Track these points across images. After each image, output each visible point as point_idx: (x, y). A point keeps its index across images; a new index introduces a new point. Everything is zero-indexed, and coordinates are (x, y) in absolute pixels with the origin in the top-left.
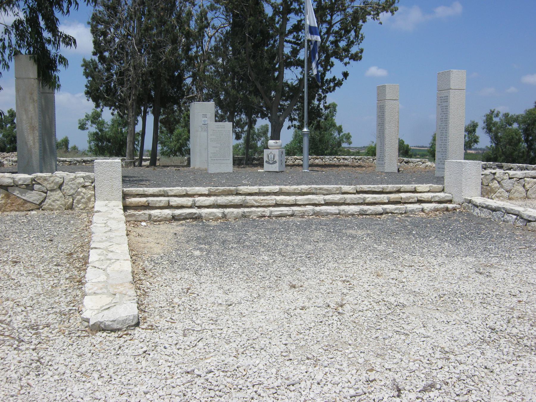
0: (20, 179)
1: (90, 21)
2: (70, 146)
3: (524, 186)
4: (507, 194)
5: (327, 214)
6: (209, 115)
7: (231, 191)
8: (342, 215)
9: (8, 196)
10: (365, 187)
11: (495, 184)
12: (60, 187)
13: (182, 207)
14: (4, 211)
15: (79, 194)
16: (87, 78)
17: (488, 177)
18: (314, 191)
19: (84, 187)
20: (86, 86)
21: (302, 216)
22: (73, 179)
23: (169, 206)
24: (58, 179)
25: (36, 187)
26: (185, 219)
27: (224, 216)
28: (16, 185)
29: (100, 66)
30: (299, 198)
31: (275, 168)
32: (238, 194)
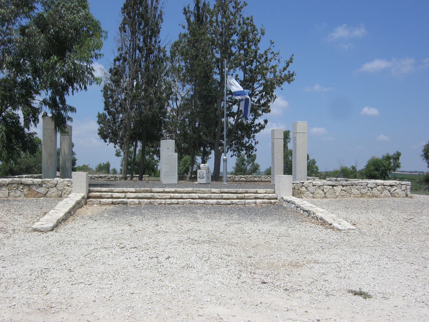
0: (36, 181)
1: (103, 89)
2: (111, 168)
3: (323, 190)
4: (312, 195)
5: (198, 203)
6: (171, 148)
7: (148, 190)
8: (206, 204)
9: (30, 190)
10: (226, 190)
11: (304, 189)
12: (56, 185)
13: (119, 198)
14: (27, 197)
15: (65, 189)
16: (99, 124)
17: (298, 185)
18: (195, 191)
19: (68, 186)
20: (99, 130)
21: (183, 204)
22: (62, 182)
23: (112, 198)
24: (54, 182)
25: (44, 185)
26: (119, 204)
27: (140, 203)
28: (34, 184)
29: (108, 117)
30: (183, 195)
31: (204, 181)
32: (151, 192)
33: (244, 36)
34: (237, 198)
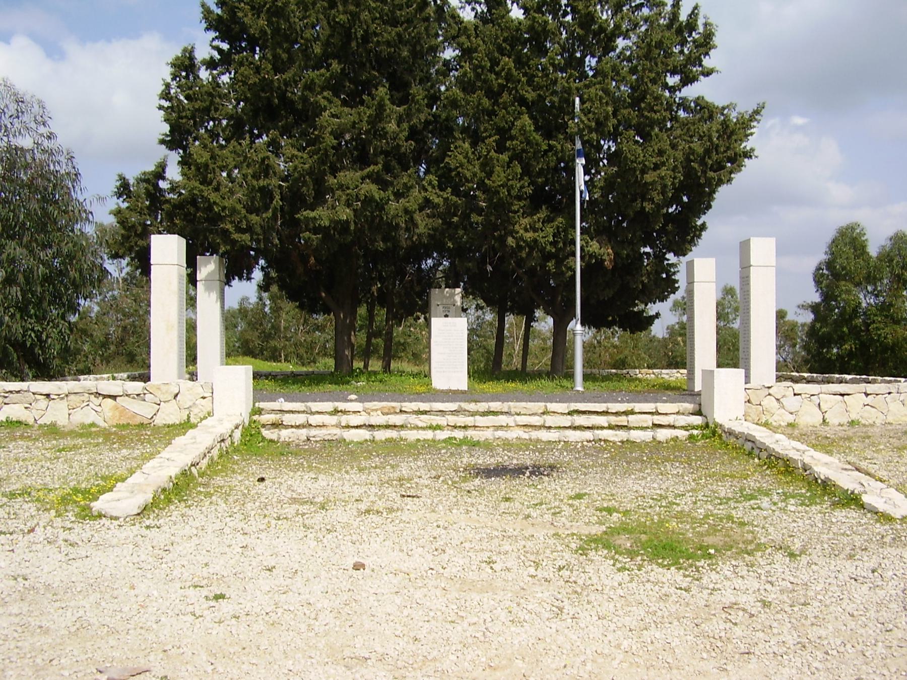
25: (148, 397)
33: (82, 428)
34: (610, 427)
